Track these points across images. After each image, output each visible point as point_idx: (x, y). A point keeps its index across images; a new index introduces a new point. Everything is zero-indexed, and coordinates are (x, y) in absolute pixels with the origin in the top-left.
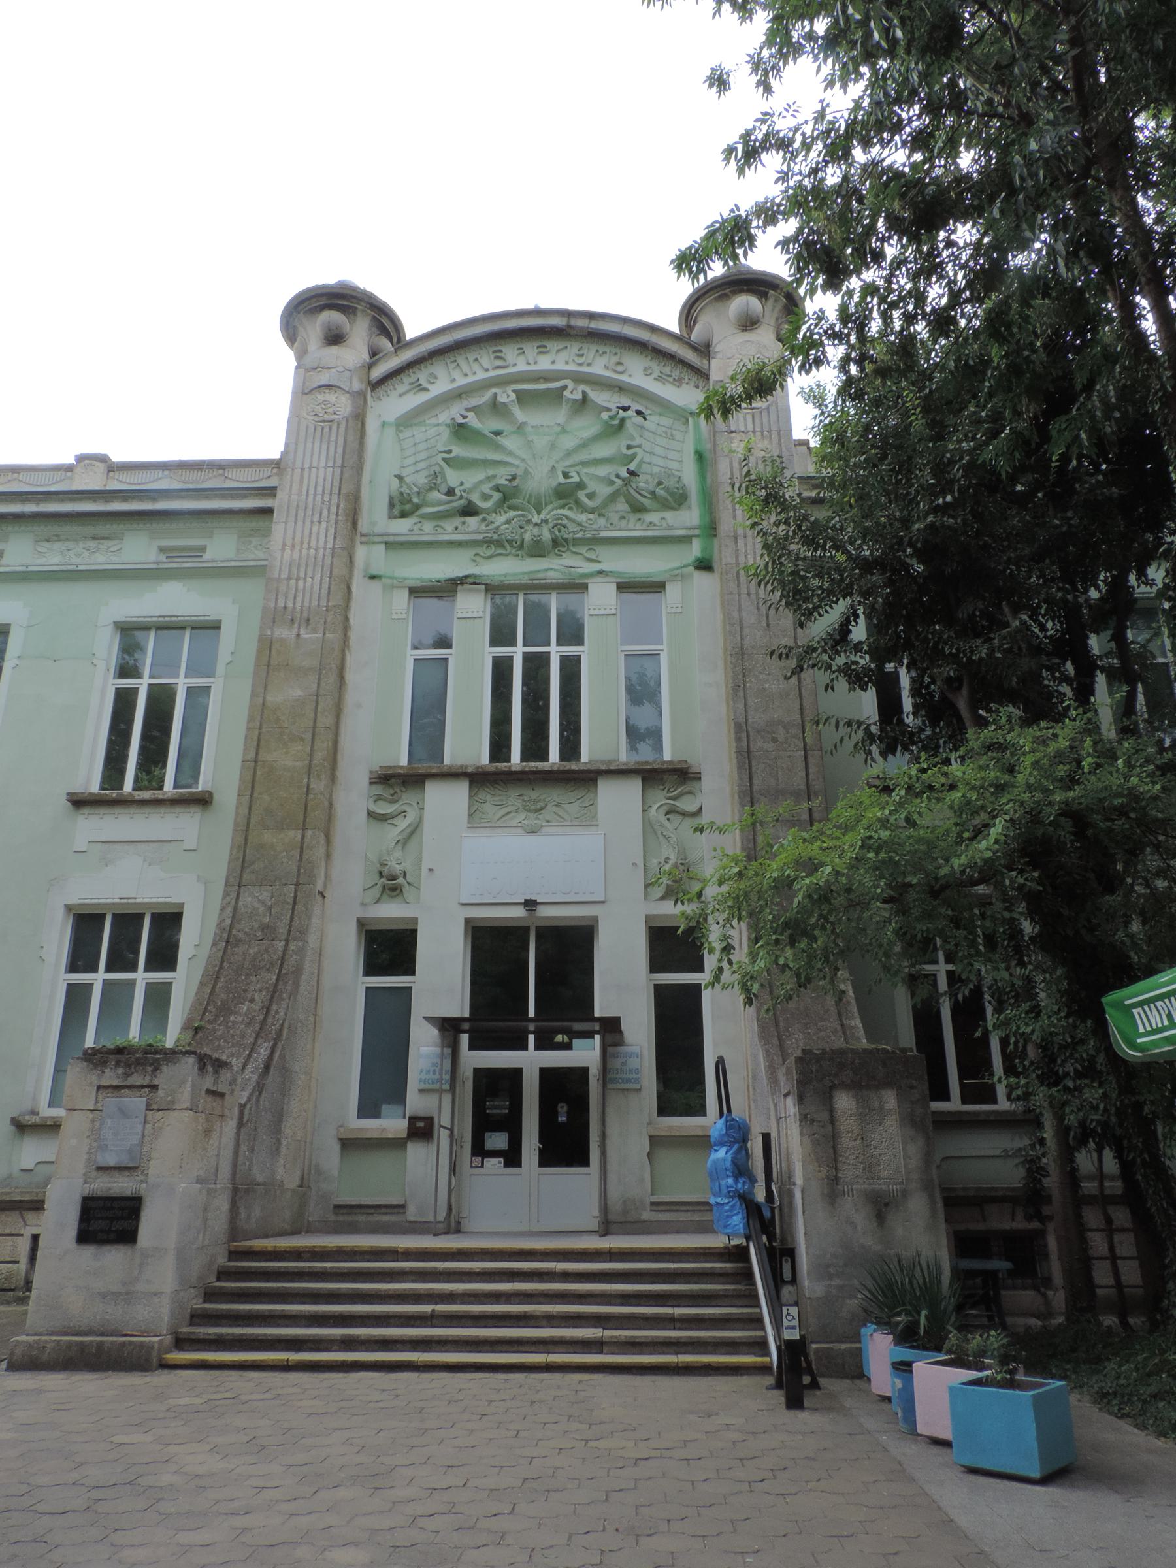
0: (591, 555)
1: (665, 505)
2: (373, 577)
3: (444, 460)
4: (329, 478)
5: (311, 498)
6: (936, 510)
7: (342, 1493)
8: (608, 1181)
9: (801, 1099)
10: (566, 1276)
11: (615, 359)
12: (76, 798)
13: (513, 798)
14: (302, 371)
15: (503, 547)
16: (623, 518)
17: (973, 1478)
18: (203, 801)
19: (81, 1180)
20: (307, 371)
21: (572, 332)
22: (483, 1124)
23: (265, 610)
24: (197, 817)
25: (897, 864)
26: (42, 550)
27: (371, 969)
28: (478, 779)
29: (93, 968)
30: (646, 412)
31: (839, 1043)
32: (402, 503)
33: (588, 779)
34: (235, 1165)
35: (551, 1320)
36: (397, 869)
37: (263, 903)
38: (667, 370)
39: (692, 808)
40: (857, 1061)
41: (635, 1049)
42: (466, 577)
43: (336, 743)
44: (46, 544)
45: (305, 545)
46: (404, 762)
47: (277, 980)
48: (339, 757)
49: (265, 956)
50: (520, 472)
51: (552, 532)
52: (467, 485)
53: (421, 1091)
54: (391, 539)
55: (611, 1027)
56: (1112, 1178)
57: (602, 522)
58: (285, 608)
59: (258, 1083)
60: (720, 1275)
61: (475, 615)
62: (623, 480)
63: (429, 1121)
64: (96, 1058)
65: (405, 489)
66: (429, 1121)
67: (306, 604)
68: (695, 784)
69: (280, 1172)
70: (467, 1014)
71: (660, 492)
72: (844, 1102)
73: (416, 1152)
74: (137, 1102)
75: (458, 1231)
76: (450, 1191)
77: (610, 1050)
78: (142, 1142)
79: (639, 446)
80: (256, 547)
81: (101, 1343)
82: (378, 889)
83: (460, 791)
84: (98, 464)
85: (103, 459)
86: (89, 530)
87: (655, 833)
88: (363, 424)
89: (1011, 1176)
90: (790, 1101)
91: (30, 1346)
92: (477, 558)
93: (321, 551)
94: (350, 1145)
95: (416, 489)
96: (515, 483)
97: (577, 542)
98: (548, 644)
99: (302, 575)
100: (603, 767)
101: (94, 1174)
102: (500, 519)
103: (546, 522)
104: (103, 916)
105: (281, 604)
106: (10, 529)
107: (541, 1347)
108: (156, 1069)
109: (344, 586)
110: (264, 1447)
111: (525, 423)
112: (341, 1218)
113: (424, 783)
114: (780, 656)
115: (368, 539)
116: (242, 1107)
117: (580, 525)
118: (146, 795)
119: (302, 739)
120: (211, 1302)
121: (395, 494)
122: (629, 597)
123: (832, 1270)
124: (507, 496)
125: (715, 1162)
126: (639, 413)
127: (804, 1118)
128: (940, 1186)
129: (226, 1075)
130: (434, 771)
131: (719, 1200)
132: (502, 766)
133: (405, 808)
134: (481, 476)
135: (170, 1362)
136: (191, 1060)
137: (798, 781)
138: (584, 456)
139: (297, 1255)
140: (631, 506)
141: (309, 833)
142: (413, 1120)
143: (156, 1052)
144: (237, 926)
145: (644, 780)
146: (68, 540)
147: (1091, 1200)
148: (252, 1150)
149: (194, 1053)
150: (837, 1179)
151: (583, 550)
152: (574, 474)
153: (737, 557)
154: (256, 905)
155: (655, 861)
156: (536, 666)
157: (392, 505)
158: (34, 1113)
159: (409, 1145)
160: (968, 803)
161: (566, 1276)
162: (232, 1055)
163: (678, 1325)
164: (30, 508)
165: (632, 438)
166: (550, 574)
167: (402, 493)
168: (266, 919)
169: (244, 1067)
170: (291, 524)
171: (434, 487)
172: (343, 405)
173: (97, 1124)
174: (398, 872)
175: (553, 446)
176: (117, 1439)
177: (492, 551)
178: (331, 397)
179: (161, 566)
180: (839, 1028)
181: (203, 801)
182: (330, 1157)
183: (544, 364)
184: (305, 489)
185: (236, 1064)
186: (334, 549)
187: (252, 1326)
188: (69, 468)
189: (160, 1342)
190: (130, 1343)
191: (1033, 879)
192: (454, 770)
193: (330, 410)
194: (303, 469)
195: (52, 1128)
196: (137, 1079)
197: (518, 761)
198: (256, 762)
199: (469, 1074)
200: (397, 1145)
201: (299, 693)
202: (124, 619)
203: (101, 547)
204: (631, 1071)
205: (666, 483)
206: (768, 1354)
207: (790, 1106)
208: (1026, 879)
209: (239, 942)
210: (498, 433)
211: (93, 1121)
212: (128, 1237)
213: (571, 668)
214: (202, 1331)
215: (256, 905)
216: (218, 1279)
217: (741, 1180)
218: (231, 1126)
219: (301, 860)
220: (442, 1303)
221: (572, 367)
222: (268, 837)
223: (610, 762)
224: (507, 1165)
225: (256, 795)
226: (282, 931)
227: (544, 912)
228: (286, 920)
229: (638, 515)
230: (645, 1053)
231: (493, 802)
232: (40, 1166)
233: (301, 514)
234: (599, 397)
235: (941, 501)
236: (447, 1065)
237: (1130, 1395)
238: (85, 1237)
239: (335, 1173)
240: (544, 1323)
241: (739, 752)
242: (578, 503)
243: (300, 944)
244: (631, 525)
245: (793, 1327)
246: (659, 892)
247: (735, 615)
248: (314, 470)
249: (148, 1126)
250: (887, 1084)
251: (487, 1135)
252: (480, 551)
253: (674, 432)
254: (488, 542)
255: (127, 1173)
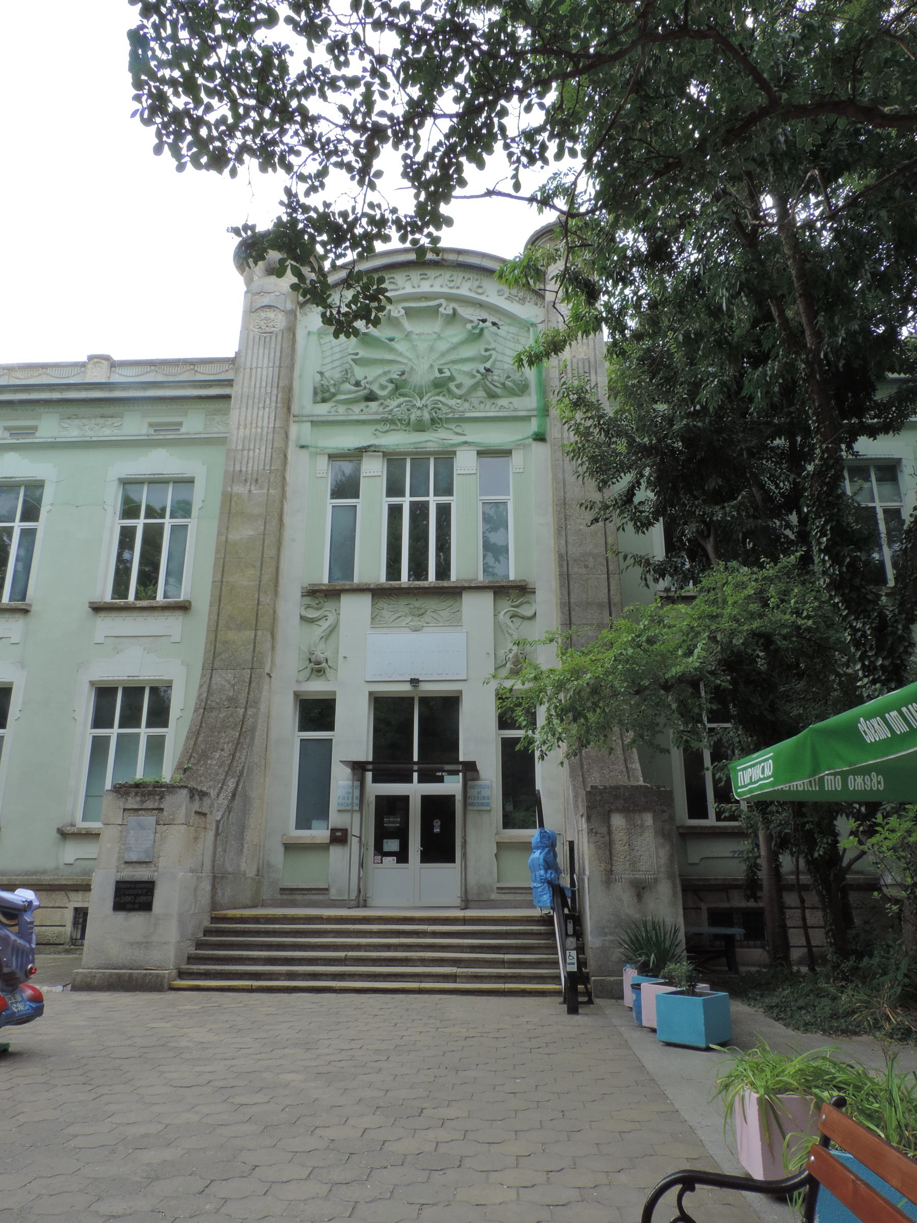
0: (459, 430)
1: (512, 393)
2: (302, 447)
3: (353, 360)
4: (270, 375)
5: (257, 390)
6: (689, 415)
7: (287, 1051)
8: (468, 872)
9: (589, 819)
10: (434, 934)
11: (477, 283)
12: (95, 606)
13: (402, 605)
14: (250, 295)
15: (396, 424)
16: (482, 402)
17: (668, 1048)
18: (184, 607)
19: (115, 870)
20: (254, 295)
21: (445, 264)
22: (381, 834)
23: (226, 472)
24: (181, 618)
25: (637, 672)
26: (66, 426)
27: (303, 727)
28: (378, 593)
29: (111, 726)
30: (500, 323)
31: (623, 780)
32: (323, 392)
33: (456, 592)
34: (214, 861)
35: (423, 962)
36: (322, 657)
37: (229, 682)
38: (514, 291)
39: (529, 613)
40: (627, 794)
41: (488, 783)
42: (369, 446)
43: (277, 568)
44: (69, 421)
45: (254, 425)
46: (325, 580)
47: (240, 735)
48: (280, 577)
49: (231, 719)
50: (407, 370)
51: (430, 414)
52: (370, 379)
53: (339, 811)
54: (315, 419)
55: (470, 769)
56: (804, 873)
57: (466, 405)
58: (241, 471)
59: (228, 806)
60: (537, 934)
61: (376, 474)
62: (482, 375)
63: (345, 831)
64: (121, 790)
65: (324, 382)
66: (345, 831)
67: (255, 468)
68: (531, 596)
69: (243, 866)
70: (371, 759)
71: (509, 383)
72: (618, 821)
73: (336, 852)
74: (149, 820)
75: (365, 906)
76: (359, 879)
77: (470, 783)
78: (154, 846)
79: (494, 349)
80: (218, 423)
81: (131, 975)
82: (308, 671)
83: (365, 602)
84: (103, 361)
85: (107, 358)
86: (98, 411)
87: (503, 631)
88: (294, 335)
89: (737, 870)
90: (584, 820)
91: (85, 975)
92: (377, 433)
93: (266, 429)
94: (290, 847)
95: (333, 382)
96: (404, 378)
97: (448, 420)
98: (428, 495)
99: (252, 447)
100: (466, 585)
101: (123, 866)
102: (393, 404)
103: (426, 406)
104: (116, 689)
105: (237, 468)
106: (42, 410)
107: (417, 979)
108: (162, 798)
109: (282, 455)
110: (240, 1030)
111: (411, 332)
112: (285, 897)
113: (339, 595)
114: (586, 508)
115: (299, 419)
116: (218, 822)
117: (450, 408)
118: (145, 603)
119: (254, 566)
120: (200, 949)
121: (318, 385)
122: (487, 460)
123: (606, 930)
124: (398, 387)
125: (533, 860)
126: (494, 324)
127: (590, 831)
128: (680, 876)
129: (207, 802)
130: (347, 587)
131: (535, 885)
132: (394, 583)
133: (326, 613)
134: (379, 371)
135: (176, 987)
136: (185, 792)
137: (603, 595)
138: (453, 356)
139: (256, 920)
140: (487, 393)
141: (259, 633)
142: (334, 831)
143: (162, 786)
144: (211, 698)
145: (494, 593)
146: (83, 418)
147: (790, 888)
148: (225, 851)
149: (186, 787)
150: (611, 871)
151: (453, 426)
152: (446, 371)
153: (562, 434)
154: (224, 683)
155: (503, 651)
156: (419, 511)
157: (315, 393)
158: (73, 825)
159: (331, 847)
160: (692, 628)
161: (434, 934)
162: (210, 787)
163: (506, 965)
164: (56, 395)
165: (489, 343)
166: (429, 444)
167: (322, 385)
168: (231, 694)
169: (218, 795)
170: (244, 409)
171: (346, 380)
172: (279, 321)
173: (124, 834)
174: (322, 659)
175: (431, 349)
176: (149, 1025)
177: (387, 427)
178: (271, 314)
179: (150, 437)
180: (624, 769)
181: (184, 607)
182: (277, 857)
183: (425, 287)
184: (253, 384)
185: (213, 793)
186: (274, 428)
187: (228, 965)
188: (83, 365)
189: (169, 974)
190: (150, 974)
191: (728, 681)
192: (361, 587)
193: (270, 325)
194: (251, 369)
195: (91, 836)
196: (149, 804)
197: (406, 580)
198: (222, 582)
199: (373, 799)
200: (322, 848)
201: (251, 533)
202: (125, 476)
203: (107, 423)
204: (484, 798)
205: (513, 377)
206: (561, 984)
207: (583, 824)
208: (723, 681)
209: (212, 709)
210: (392, 340)
211: (121, 832)
212: (147, 907)
213: (444, 512)
214: (195, 968)
215: (224, 683)
216: (205, 935)
217: (549, 872)
218: (211, 834)
219: (254, 651)
220: (352, 951)
221: (445, 290)
222: (231, 635)
223: (471, 581)
224: (398, 862)
225: (222, 605)
226: (243, 701)
227: (425, 687)
228: (244, 694)
229: (493, 400)
230: (494, 785)
231: (389, 609)
232: (78, 862)
233: (250, 402)
234: (466, 312)
235: (692, 409)
236: (357, 793)
237: (786, 1007)
238: (119, 906)
239: (281, 867)
240: (419, 964)
241: (561, 575)
242: (449, 391)
243: (255, 710)
244: (487, 408)
245: (573, 964)
246: (505, 672)
247: (560, 476)
248: (259, 370)
249: (158, 835)
250: (645, 809)
251: (385, 841)
252: (379, 427)
253: (520, 338)
254: (385, 421)
255: (144, 865)
